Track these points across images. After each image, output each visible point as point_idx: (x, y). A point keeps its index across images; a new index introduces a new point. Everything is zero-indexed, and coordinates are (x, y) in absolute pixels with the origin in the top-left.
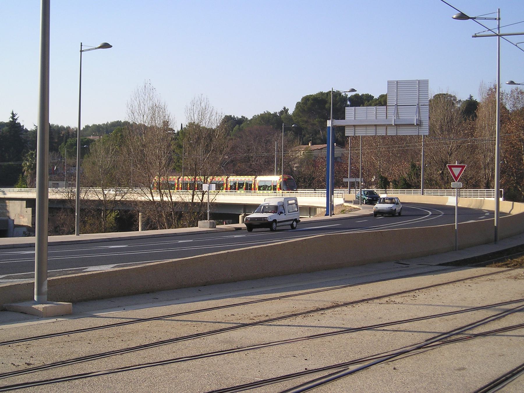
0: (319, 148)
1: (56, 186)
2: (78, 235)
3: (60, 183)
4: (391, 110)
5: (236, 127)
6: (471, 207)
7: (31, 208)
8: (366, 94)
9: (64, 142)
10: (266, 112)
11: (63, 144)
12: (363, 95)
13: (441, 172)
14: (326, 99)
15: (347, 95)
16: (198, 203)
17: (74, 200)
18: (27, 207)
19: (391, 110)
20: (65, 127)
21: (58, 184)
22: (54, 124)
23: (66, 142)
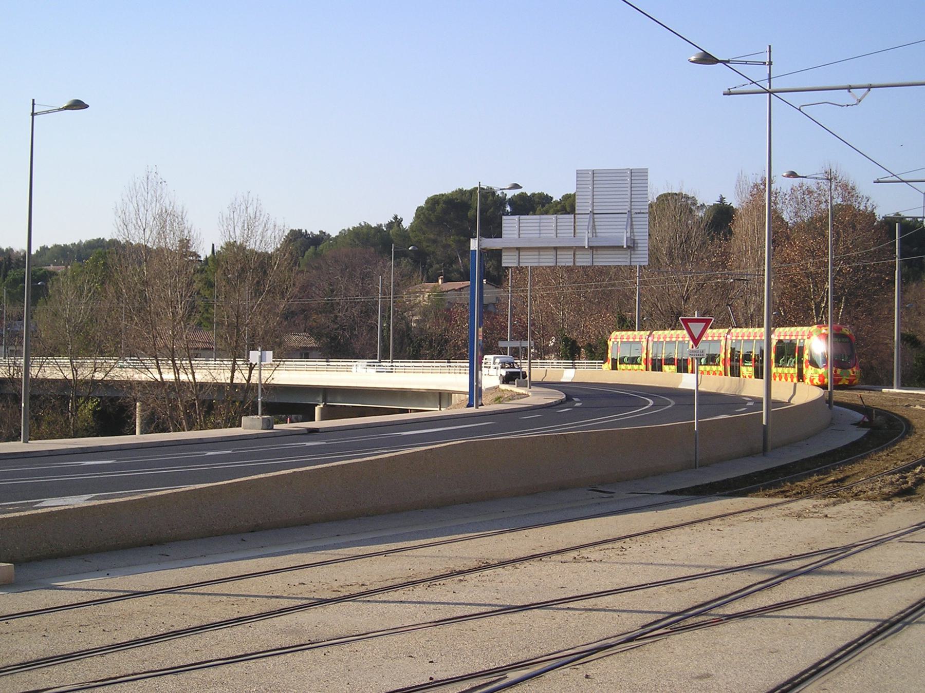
6: (722, 392)
8: (539, 194)
10: (363, 224)
12: (533, 195)
17: (20, 380)
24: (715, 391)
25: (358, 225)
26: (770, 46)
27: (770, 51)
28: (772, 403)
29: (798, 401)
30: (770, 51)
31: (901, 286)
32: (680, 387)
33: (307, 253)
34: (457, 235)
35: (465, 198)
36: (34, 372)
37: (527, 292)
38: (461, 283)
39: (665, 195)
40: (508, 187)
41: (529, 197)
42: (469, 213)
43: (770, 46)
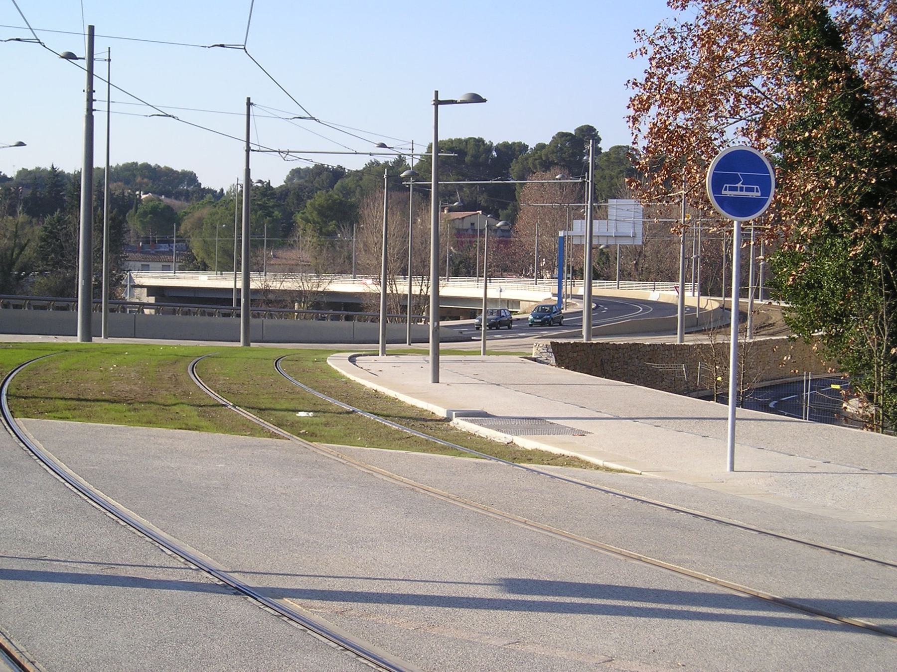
0: (460, 217)
1: (145, 268)
2: (106, 337)
3: (152, 264)
4: (612, 224)
5: (337, 183)
6: (669, 302)
7: (154, 297)
8: (518, 143)
9: (134, 209)
10: (373, 161)
11: (132, 211)
12: (514, 144)
13: (635, 262)
14: (465, 150)
15: (492, 143)
16: (417, 296)
17: (427, 297)
18: (148, 296)
19: (612, 224)
20: (66, 173)
21: (169, 266)
22: (40, 166)
23: (137, 209)
24: (656, 300)
25: (49, 169)
26: (109, 48)
27: (109, 52)
28: (700, 309)
29: (709, 308)
30: (109, 52)
31: (110, 229)
32: (649, 299)
33: (336, 186)
34: (457, 175)
35: (462, 146)
36: (444, 292)
37: (94, 227)
38: (462, 213)
39: (619, 147)
40: (14, 144)
41: (510, 145)
42: (466, 158)
43: (109, 48)
